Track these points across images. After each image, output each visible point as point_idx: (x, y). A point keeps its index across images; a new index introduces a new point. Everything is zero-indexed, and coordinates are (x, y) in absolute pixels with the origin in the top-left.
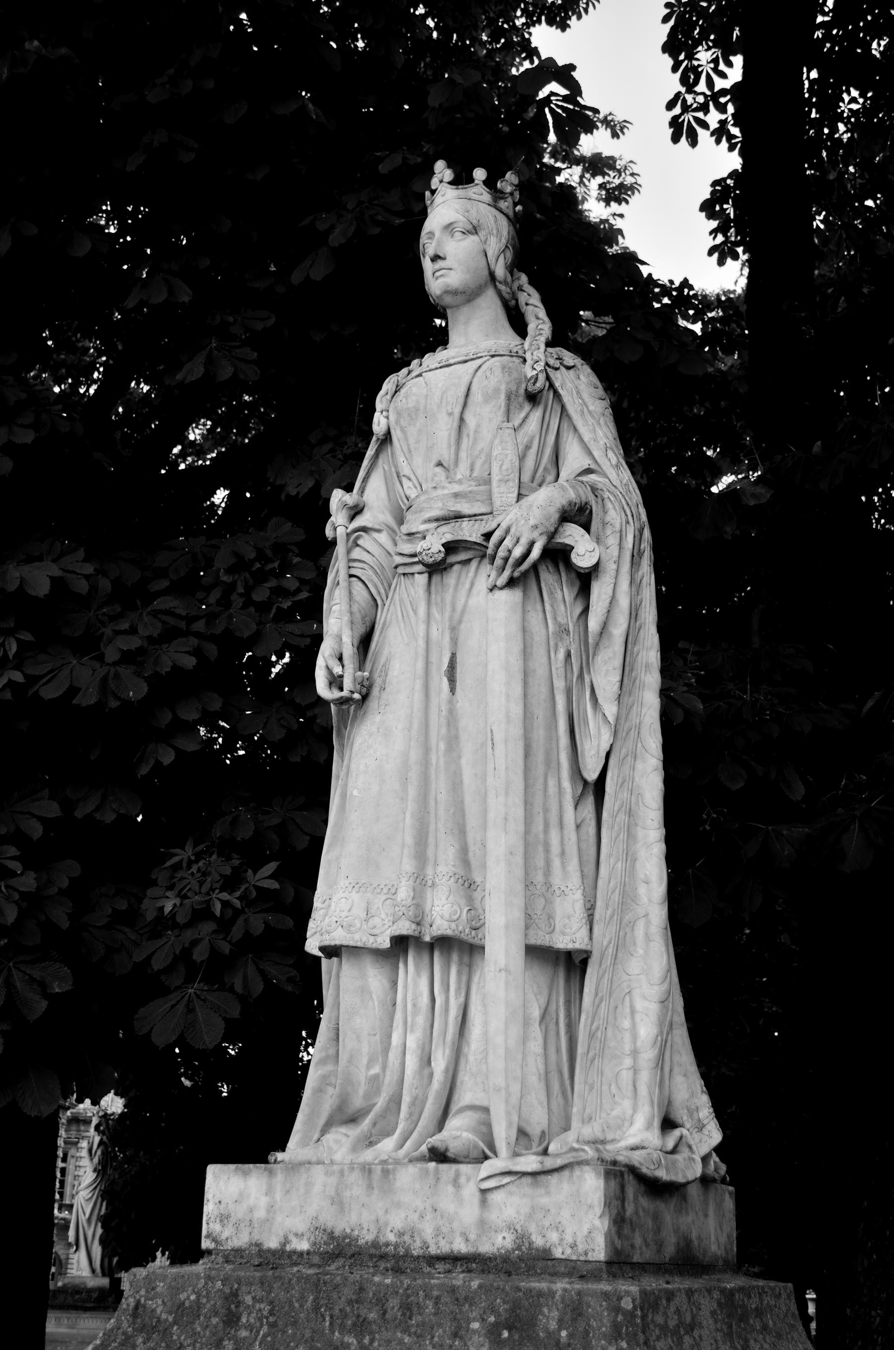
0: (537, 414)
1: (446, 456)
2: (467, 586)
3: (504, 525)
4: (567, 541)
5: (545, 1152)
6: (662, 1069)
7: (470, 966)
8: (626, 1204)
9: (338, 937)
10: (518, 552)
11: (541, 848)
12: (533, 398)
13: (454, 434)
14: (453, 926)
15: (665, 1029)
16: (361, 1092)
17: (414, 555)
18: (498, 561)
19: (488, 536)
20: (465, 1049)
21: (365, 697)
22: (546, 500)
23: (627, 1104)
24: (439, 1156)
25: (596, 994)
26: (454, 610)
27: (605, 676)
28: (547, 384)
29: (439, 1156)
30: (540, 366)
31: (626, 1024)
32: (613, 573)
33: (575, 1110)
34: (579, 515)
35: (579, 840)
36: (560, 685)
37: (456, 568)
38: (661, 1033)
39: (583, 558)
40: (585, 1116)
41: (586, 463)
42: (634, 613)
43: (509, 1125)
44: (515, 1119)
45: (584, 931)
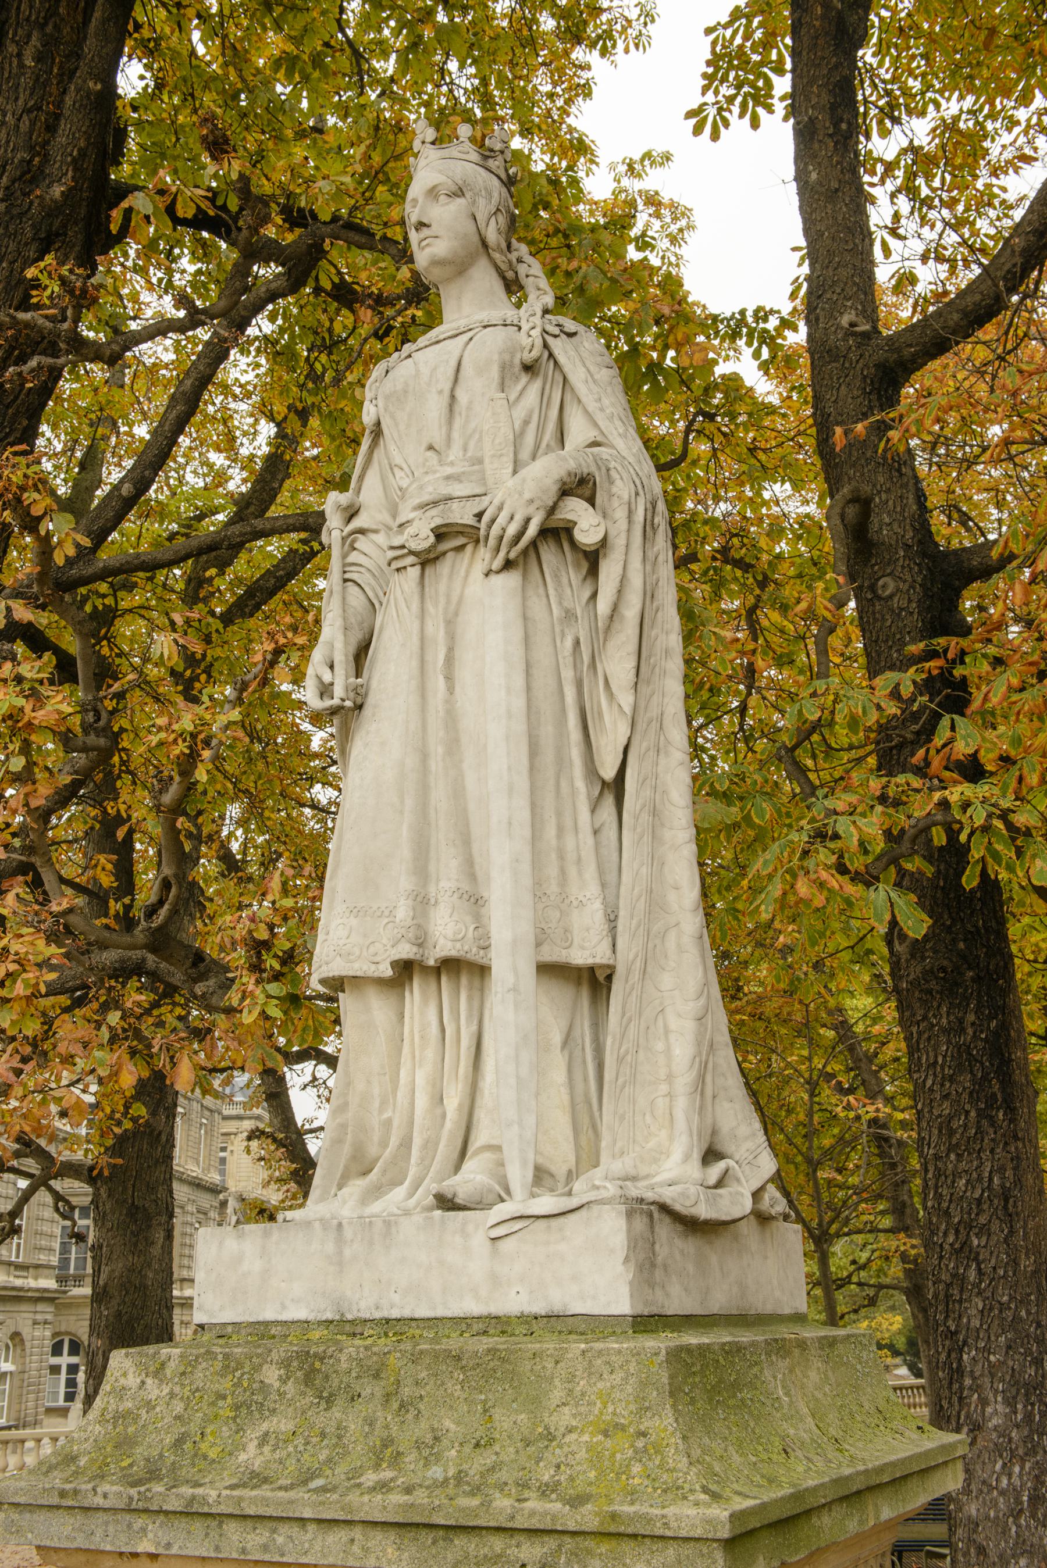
0: (537, 384)
1: (437, 437)
2: (462, 573)
3: (496, 502)
4: (570, 516)
5: (570, 1194)
6: (702, 1094)
7: (482, 990)
8: (657, 1247)
9: (337, 968)
10: (512, 530)
11: (554, 856)
12: (529, 368)
13: (445, 410)
14: (458, 945)
15: (705, 1051)
16: (376, 1139)
17: (403, 547)
18: (492, 542)
19: (479, 516)
20: (481, 1084)
21: (360, 707)
22: (545, 472)
23: (664, 1134)
24: (446, 1203)
25: (624, 1014)
26: (448, 602)
27: (618, 664)
28: (546, 354)
29: (446, 1203)
30: (536, 333)
31: (660, 1046)
32: (623, 549)
33: (603, 1144)
34: (580, 487)
35: (597, 845)
36: (568, 674)
37: (450, 555)
38: (700, 1053)
39: (587, 534)
40: (617, 1150)
41: (592, 435)
42: (650, 594)
43: (524, 1163)
44: (531, 1156)
45: (606, 944)
